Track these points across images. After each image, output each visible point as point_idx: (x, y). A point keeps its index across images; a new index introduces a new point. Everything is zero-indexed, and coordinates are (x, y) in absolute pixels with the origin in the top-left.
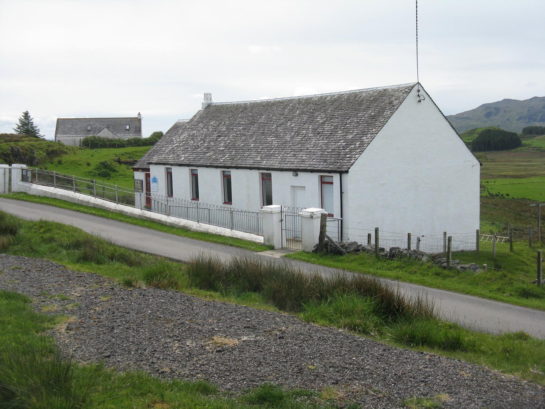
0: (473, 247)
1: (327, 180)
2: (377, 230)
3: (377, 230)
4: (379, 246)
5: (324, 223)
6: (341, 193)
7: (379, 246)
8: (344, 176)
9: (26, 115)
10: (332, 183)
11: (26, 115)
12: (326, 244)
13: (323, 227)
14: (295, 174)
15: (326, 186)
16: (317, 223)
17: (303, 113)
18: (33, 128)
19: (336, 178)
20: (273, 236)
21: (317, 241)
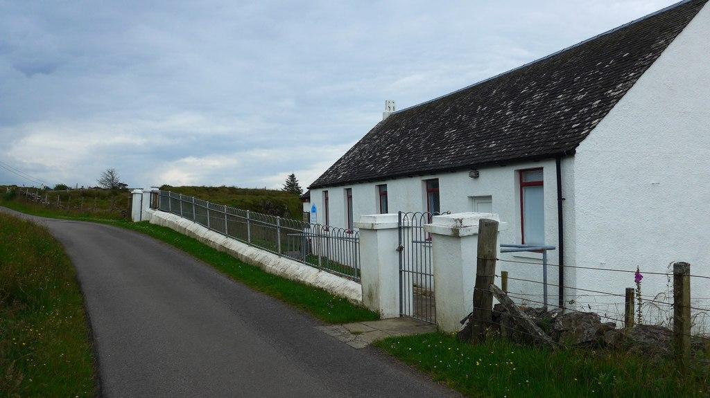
0: (547, 263)
1: (532, 178)
2: (681, 274)
3: (681, 274)
4: (693, 331)
5: (487, 249)
6: (561, 200)
7: (693, 331)
8: (567, 165)
9: (292, 177)
10: (541, 184)
11: (292, 177)
12: (496, 317)
13: (486, 262)
14: (473, 174)
15: (529, 194)
16: (469, 251)
17: (502, 91)
18: (297, 188)
19: (549, 170)
20: (377, 285)
21: (469, 307)
